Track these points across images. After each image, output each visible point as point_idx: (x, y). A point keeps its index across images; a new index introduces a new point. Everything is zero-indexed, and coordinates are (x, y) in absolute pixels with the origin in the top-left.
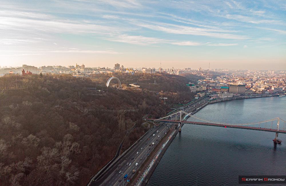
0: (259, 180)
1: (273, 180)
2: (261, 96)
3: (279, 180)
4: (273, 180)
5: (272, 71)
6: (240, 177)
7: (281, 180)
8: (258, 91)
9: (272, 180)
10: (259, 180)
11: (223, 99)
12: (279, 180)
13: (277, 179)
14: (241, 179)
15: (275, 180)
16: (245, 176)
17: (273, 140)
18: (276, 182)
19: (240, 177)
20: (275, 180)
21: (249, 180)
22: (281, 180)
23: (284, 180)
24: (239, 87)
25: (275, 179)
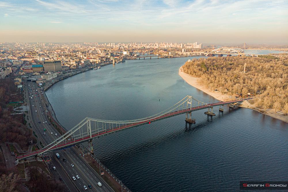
0: (261, 185)
1: (274, 186)
2: (80, 72)
3: (281, 186)
4: (274, 186)
5: (51, 43)
6: (242, 183)
7: (283, 186)
8: (73, 67)
9: (273, 186)
10: (261, 185)
11: (53, 82)
12: (281, 186)
13: (279, 185)
14: (242, 186)
15: (276, 185)
16: (273, 182)
17: (185, 121)
18: (255, 188)
19: (242, 183)
20: (276, 185)
21: (250, 186)
22: (283, 186)
23: (286, 186)
24: (56, 64)
25: (277, 185)
